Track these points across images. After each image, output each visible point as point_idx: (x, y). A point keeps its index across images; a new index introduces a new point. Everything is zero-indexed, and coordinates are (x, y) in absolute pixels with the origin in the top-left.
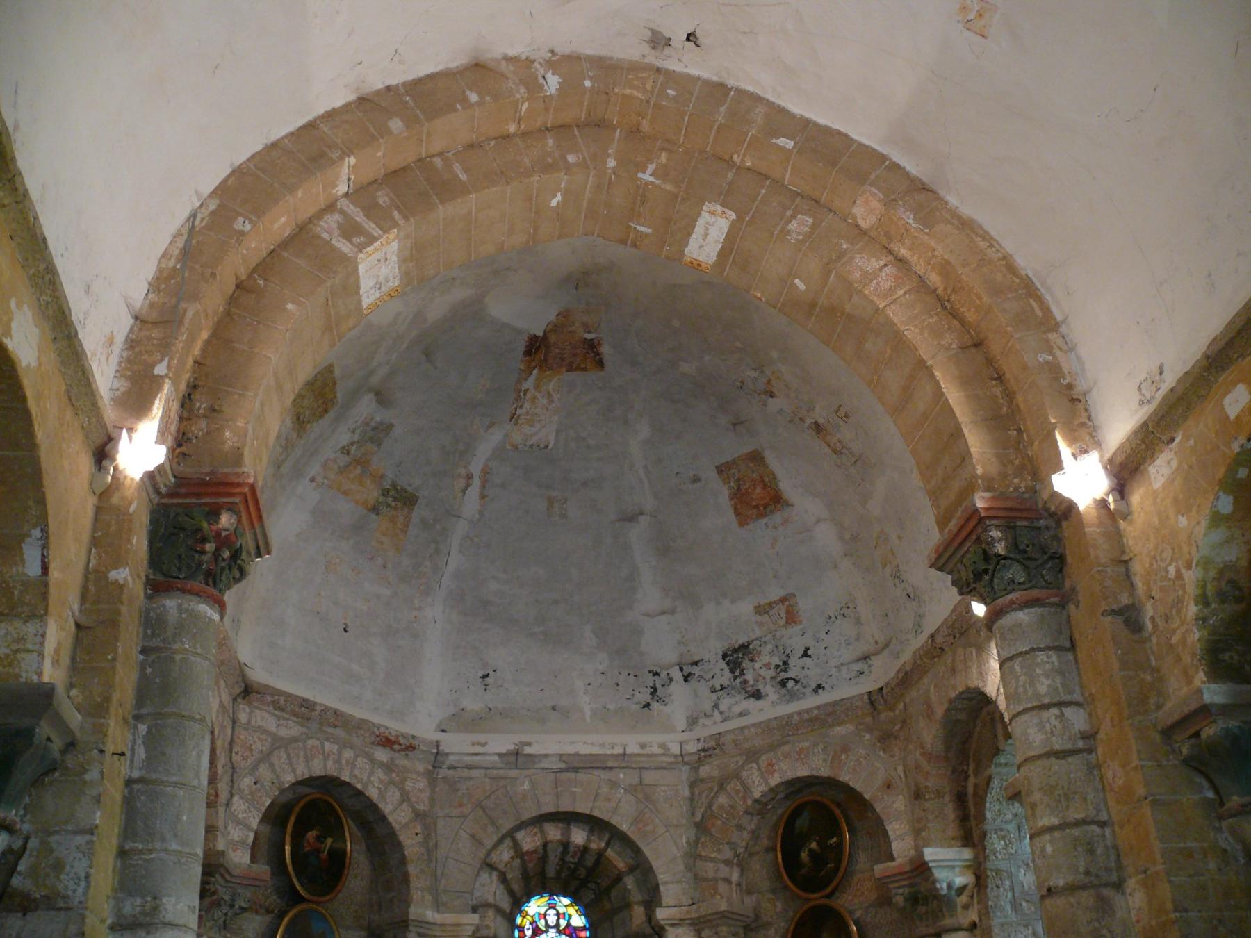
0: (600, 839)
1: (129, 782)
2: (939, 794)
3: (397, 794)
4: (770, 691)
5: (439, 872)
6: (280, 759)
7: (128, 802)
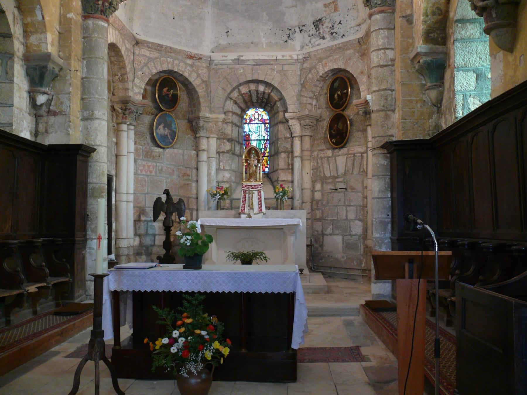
1: (82, 78)
3: (196, 75)
4: (328, 37)
7: (83, 84)
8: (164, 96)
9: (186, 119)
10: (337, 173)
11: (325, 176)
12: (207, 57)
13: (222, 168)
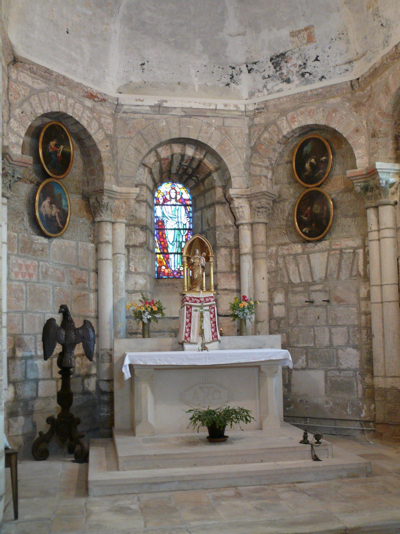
0: (201, 154)
2: (386, 135)
3: (97, 124)
5: (118, 166)
6: (35, 100)
8: (50, 154)
9: (79, 194)
10: (312, 278)
11: (291, 282)
12: (113, 99)
13: (133, 271)
